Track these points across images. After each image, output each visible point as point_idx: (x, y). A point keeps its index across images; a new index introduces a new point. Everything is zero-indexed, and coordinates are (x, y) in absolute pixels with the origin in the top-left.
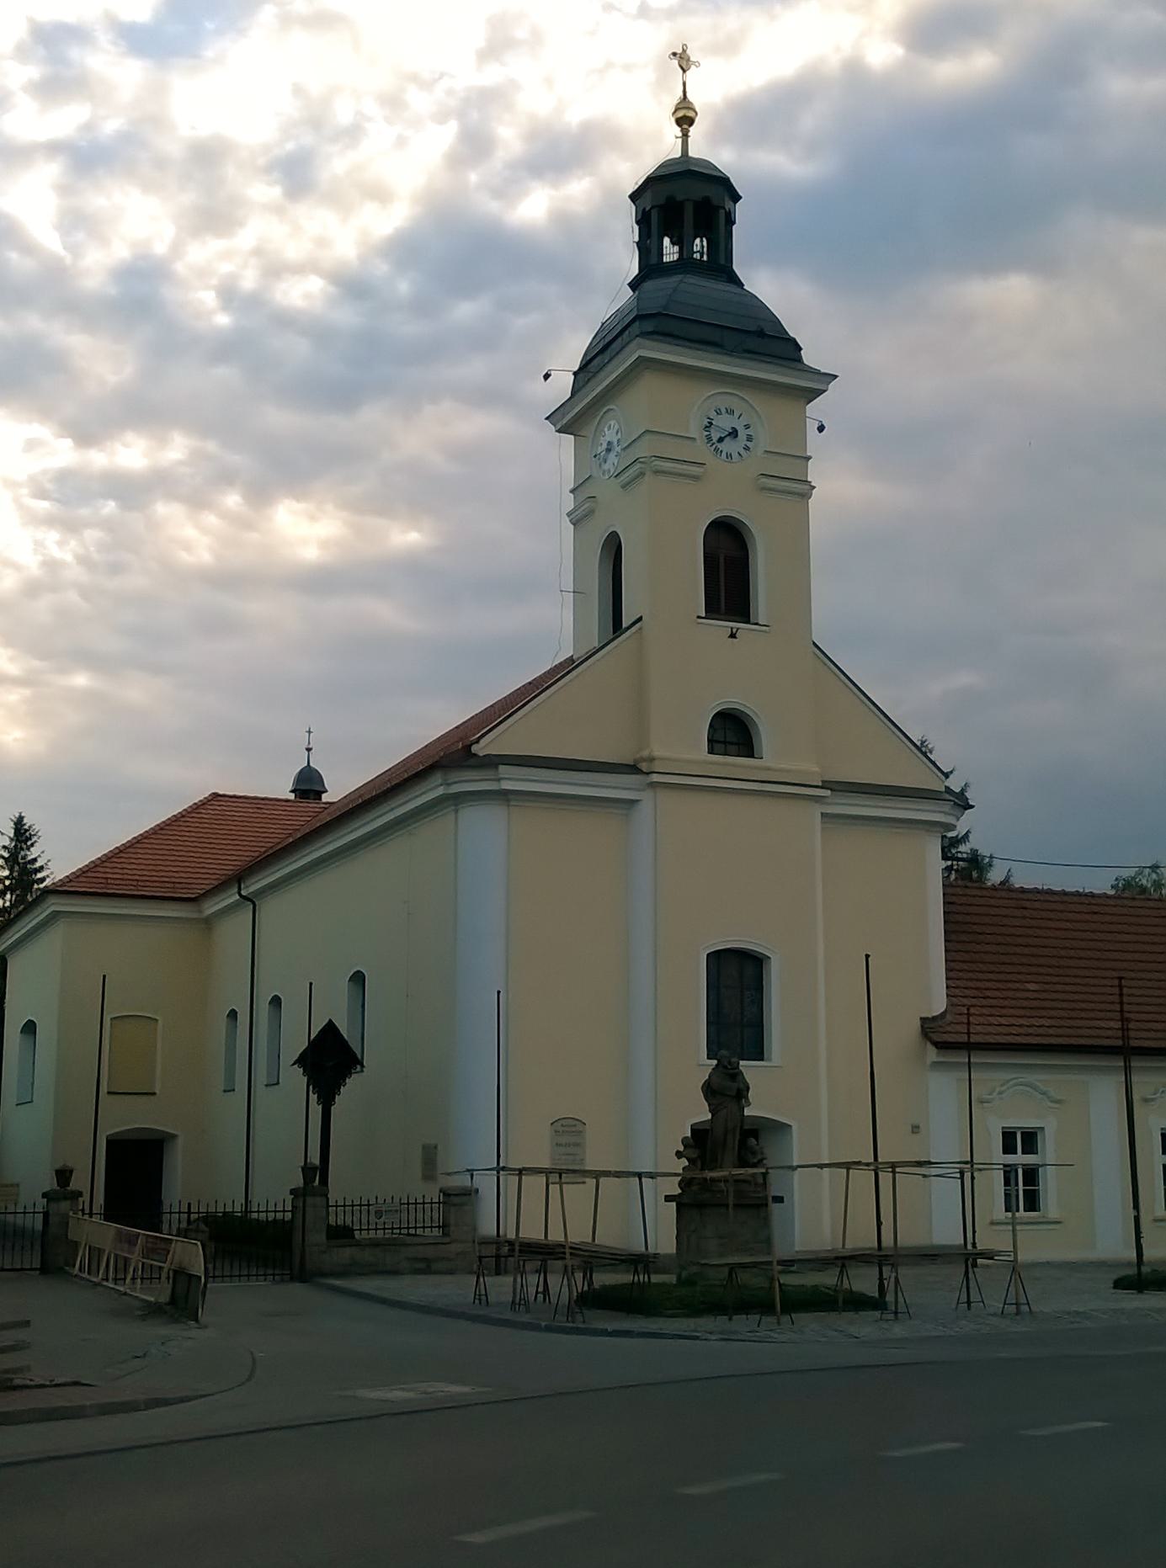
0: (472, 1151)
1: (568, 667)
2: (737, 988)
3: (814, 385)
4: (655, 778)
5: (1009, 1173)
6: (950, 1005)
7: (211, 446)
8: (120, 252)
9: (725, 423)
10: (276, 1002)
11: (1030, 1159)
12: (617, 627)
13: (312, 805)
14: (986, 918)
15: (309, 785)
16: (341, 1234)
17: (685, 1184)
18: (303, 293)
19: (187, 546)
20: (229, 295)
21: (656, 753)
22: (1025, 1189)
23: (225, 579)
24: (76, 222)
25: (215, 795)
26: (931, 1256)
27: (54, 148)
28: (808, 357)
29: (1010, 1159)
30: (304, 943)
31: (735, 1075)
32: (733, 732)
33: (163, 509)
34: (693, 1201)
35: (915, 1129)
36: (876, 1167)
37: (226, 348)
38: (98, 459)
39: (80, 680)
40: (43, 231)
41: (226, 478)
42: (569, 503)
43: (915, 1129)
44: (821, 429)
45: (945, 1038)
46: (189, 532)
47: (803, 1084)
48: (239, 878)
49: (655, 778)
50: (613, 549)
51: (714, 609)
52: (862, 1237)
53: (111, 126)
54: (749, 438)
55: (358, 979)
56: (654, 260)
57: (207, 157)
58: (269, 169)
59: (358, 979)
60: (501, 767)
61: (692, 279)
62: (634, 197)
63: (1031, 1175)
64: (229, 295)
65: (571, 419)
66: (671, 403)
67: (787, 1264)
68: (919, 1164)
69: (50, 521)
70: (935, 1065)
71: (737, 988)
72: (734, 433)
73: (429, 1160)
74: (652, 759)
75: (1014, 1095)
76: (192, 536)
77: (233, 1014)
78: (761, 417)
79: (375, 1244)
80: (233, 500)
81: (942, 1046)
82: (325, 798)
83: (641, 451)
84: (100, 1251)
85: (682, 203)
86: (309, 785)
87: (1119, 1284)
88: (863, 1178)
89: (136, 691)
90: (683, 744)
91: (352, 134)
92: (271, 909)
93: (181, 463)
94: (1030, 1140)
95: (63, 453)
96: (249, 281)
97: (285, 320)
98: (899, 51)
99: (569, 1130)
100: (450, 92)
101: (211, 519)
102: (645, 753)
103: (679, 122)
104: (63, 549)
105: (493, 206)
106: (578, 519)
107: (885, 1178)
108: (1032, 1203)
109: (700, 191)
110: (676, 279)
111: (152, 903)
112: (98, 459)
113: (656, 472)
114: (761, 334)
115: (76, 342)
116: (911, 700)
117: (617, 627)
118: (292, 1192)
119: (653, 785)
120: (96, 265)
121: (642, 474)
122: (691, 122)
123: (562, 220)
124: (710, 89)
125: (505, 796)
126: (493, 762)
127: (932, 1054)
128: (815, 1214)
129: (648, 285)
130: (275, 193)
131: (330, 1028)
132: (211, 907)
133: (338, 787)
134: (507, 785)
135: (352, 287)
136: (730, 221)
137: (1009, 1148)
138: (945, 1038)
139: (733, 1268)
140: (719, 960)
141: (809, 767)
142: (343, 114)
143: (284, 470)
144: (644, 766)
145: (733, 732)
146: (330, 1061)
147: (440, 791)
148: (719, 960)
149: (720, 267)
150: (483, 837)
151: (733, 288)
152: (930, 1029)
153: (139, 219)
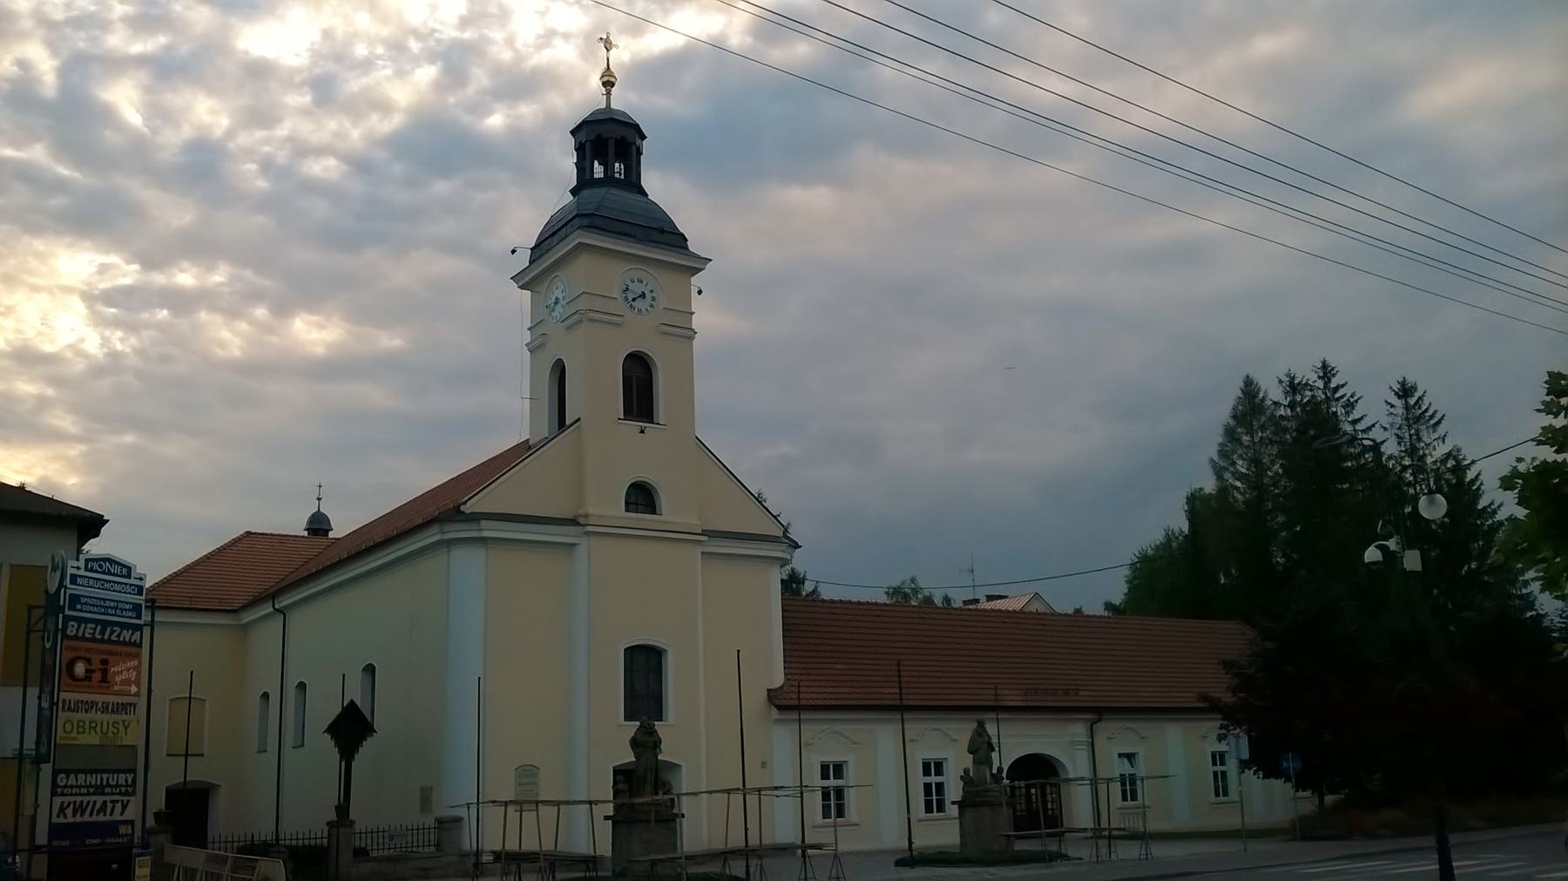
0: (458, 793)
1: (523, 450)
2: (645, 671)
3: (697, 265)
4: (590, 529)
5: (927, 787)
6: (787, 680)
7: (248, 274)
8: (186, 132)
9: (637, 288)
10: (302, 686)
11: (839, 782)
12: (562, 424)
13: (319, 540)
14: (809, 620)
15: (319, 525)
16: (361, 853)
17: (617, 808)
18: (324, 168)
19: (222, 344)
20: (267, 166)
21: (591, 511)
22: (835, 803)
23: (253, 368)
24: (158, 113)
25: (249, 533)
26: (782, 850)
27: (141, 61)
28: (692, 246)
29: (826, 783)
30: (325, 644)
31: (652, 732)
32: (642, 497)
33: (203, 316)
34: (623, 820)
35: (764, 765)
36: (744, 791)
37: (264, 204)
38: (158, 279)
39: (128, 439)
40: (133, 116)
41: (256, 296)
42: (527, 337)
43: (764, 765)
44: (700, 292)
45: (783, 703)
46: (226, 334)
47: (695, 739)
48: (273, 596)
49: (590, 529)
50: (560, 371)
51: (629, 413)
52: (737, 841)
53: (184, 50)
54: (653, 299)
55: (370, 670)
56: (588, 176)
57: (259, 71)
58: (303, 83)
59: (370, 670)
60: (483, 522)
61: (614, 191)
62: (573, 132)
63: (839, 792)
64: (267, 166)
65: (526, 281)
66: (599, 274)
67: (692, 858)
68: (776, 788)
69: (116, 323)
70: (777, 720)
71: (645, 671)
72: (643, 295)
73: (426, 800)
74: (586, 516)
75: (830, 739)
76: (228, 338)
77: (266, 696)
78: (660, 283)
79: (389, 859)
80: (261, 312)
81: (780, 708)
82: (331, 535)
83: (582, 305)
84: (194, 871)
85: (607, 140)
86: (319, 525)
87: (899, 863)
88: (737, 799)
89: (173, 449)
90: (609, 505)
91: (367, 65)
92: (297, 619)
93: (222, 284)
94: (839, 770)
95: (128, 274)
96: (282, 157)
97: (312, 187)
98: (749, 40)
99: (528, 774)
100: (439, 41)
101: (243, 326)
102: (581, 512)
103: (604, 84)
104: (120, 341)
105: (467, 119)
106: (534, 349)
107: (752, 800)
108: (840, 812)
109: (619, 132)
110: (604, 190)
111: (180, 613)
112: (158, 279)
113: (591, 320)
114: (662, 231)
115: (139, 190)
116: (748, 461)
117: (562, 424)
118: (328, 824)
119: (587, 533)
120: (172, 140)
121: (580, 321)
122: (613, 85)
123: (515, 133)
124: (624, 53)
125: (484, 541)
126: (476, 518)
127: (775, 713)
128: (702, 826)
129: (585, 193)
130: (305, 99)
131: (352, 703)
132: (248, 617)
133: (339, 530)
134: (485, 534)
135: (359, 165)
136: (639, 153)
137: (825, 776)
138: (783, 703)
139: (654, 863)
140: (632, 653)
141: (694, 522)
142: (361, 50)
143: (302, 292)
144: (582, 521)
145: (642, 497)
146: (351, 728)
147: (438, 537)
148: (632, 653)
149: (633, 183)
150: (467, 572)
151: (639, 197)
152: (772, 695)
153: (207, 113)
